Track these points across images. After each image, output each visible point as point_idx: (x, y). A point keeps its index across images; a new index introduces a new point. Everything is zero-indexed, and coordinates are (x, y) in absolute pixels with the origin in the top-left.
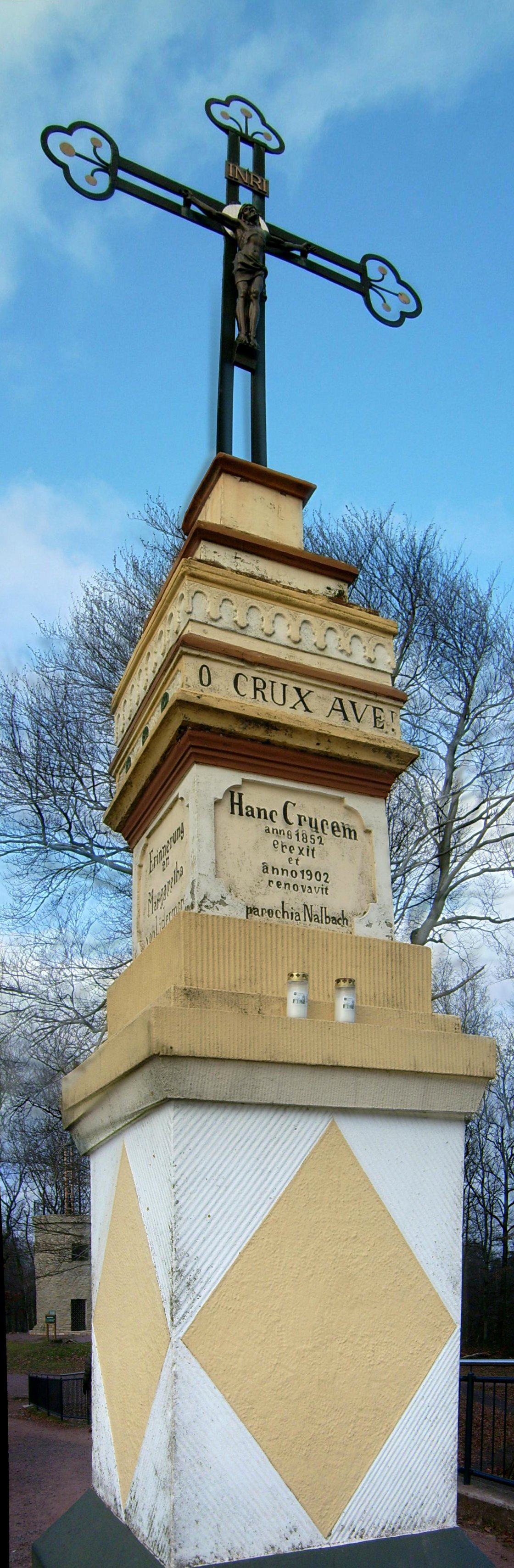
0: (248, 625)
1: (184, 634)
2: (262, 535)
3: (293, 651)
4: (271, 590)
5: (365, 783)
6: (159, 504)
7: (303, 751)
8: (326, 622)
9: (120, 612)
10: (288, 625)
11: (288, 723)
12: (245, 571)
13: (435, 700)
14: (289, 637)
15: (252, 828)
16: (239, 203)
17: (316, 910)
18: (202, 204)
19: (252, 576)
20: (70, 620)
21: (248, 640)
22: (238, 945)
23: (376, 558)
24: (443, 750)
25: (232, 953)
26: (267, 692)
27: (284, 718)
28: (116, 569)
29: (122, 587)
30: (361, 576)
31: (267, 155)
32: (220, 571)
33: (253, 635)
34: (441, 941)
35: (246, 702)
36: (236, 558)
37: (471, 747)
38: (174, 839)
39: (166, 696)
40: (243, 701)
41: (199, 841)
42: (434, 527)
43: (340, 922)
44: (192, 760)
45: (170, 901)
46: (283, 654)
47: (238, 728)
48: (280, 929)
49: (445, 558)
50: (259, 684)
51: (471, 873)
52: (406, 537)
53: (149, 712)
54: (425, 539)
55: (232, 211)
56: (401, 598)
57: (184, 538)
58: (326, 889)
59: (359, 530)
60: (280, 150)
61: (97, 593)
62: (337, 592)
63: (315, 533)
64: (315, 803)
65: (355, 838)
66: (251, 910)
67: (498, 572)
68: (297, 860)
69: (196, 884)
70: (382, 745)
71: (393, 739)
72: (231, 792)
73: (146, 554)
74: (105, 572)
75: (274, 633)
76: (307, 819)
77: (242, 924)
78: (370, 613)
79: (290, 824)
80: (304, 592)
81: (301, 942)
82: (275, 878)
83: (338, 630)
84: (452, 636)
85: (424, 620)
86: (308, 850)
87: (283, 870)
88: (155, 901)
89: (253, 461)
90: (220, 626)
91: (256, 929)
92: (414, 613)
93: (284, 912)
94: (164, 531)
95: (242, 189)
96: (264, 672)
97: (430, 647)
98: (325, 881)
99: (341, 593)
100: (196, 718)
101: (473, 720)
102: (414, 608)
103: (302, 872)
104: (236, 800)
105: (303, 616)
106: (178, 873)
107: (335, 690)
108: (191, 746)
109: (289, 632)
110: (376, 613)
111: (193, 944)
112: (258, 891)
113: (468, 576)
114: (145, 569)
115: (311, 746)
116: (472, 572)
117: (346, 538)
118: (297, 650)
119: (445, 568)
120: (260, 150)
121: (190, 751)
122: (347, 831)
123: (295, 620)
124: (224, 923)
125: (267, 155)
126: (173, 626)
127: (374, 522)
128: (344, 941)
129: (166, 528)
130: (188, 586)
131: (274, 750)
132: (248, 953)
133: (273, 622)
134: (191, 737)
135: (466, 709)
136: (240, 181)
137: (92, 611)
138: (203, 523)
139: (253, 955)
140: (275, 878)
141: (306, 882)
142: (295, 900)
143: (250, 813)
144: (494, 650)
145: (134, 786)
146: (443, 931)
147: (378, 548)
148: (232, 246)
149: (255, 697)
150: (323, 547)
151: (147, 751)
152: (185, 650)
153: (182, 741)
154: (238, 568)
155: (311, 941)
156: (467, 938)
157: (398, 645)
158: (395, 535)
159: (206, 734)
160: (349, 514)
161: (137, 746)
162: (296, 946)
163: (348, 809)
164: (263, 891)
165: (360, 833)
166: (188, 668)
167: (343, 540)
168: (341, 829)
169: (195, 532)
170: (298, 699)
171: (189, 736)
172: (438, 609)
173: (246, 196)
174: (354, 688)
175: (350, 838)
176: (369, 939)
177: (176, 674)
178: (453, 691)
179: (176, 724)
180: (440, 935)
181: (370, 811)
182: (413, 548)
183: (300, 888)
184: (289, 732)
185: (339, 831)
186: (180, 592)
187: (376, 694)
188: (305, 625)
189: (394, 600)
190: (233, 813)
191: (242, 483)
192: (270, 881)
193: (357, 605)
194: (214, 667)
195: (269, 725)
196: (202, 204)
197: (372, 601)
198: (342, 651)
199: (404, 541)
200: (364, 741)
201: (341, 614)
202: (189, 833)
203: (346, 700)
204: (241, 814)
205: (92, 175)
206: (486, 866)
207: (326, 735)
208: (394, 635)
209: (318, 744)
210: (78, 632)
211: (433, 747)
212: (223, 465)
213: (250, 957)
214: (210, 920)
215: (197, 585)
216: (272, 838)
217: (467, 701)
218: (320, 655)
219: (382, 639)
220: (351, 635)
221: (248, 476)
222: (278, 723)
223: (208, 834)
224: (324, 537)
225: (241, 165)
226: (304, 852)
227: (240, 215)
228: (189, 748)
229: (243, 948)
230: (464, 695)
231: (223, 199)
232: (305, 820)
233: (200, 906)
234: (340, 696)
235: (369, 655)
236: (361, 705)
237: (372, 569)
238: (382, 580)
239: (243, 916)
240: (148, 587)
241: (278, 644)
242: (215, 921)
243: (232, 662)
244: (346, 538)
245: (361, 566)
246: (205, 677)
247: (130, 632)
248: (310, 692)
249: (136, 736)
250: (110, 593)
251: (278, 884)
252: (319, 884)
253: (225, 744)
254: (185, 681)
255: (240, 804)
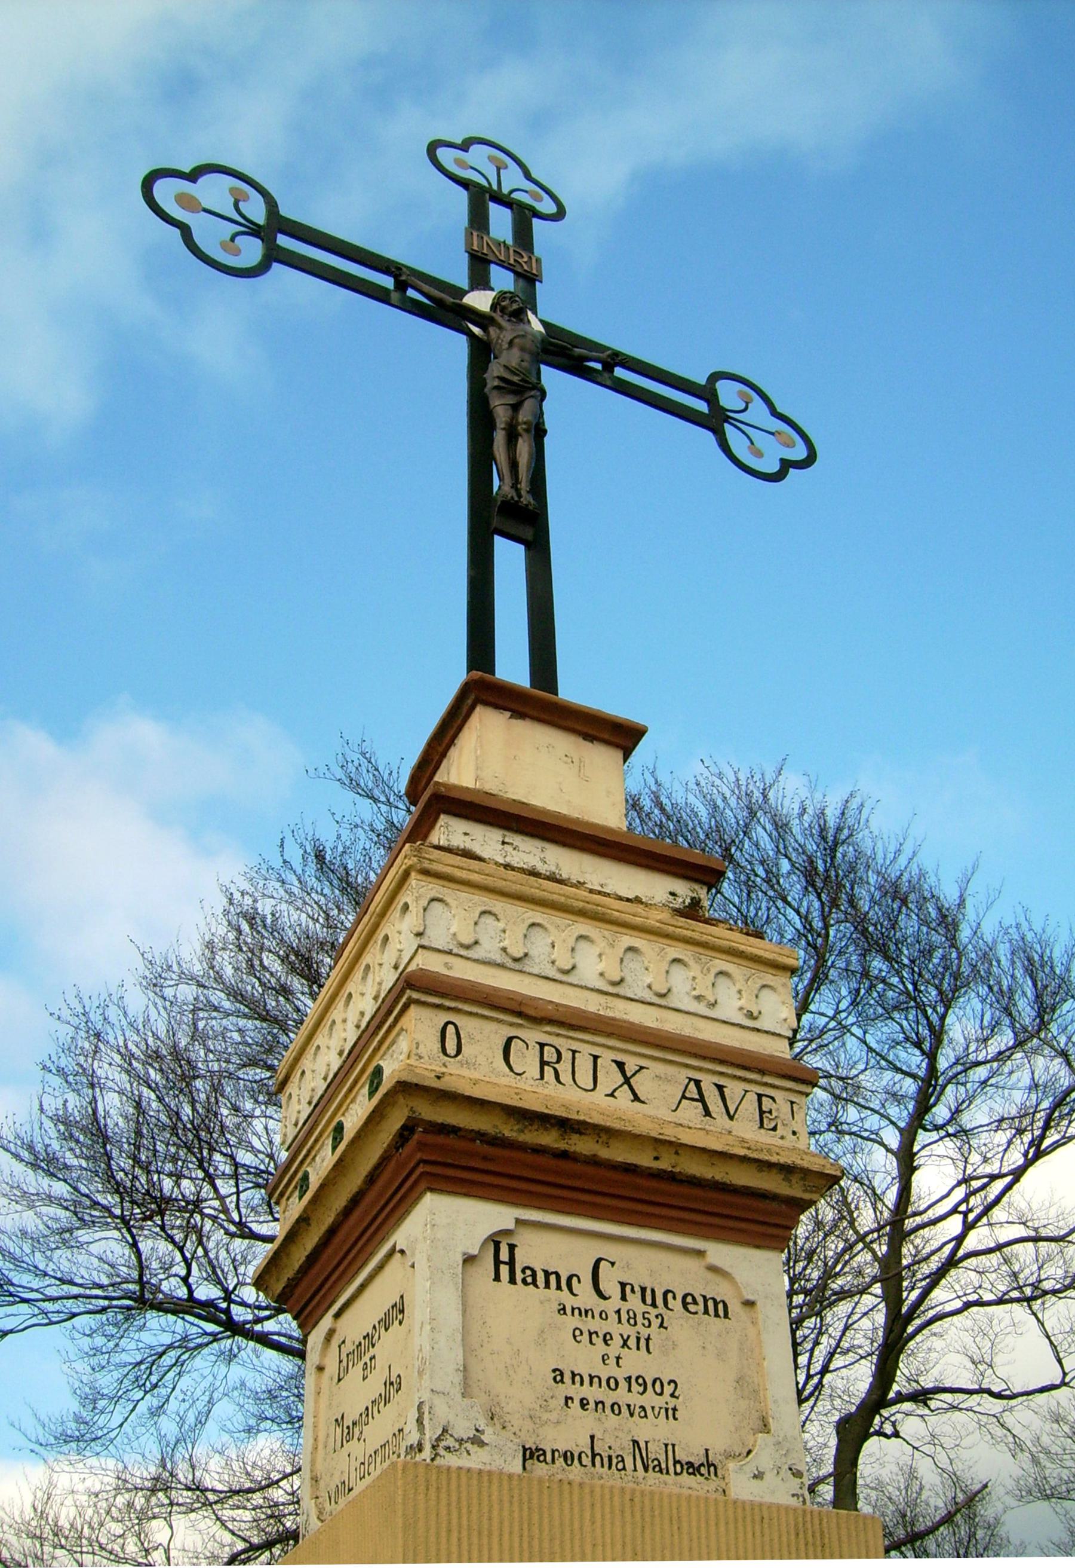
0: (526, 955)
1: (409, 969)
2: (552, 806)
3: (610, 998)
4: (568, 897)
5: (743, 1225)
6: (363, 754)
7: (630, 1169)
8: (668, 949)
9: (290, 933)
10: (600, 955)
11: (603, 1123)
12: (521, 865)
13: (870, 1057)
14: (601, 974)
15: (537, 1301)
16: (492, 289)
17: (656, 1451)
18: (426, 288)
19: (534, 873)
20: (198, 947)
21: (527, 980)
22: (506, 1524)
23: (757, 845)
24: (893, 1139)
25: (495, 1539)
26: (564, 1067)
27: (594, 1114)
28: (285, 862)
29: (296, 891)
30: (730, 875)
31: (536, 222)
32: (474, 864)
33: (536, 971)
34: (896, 1434)
35: (525, 1084)
36: (503, 843)
37: (942, 1133)
38: (386, 1323)
39: (378, 1071)
40: (522, 1084)
41: (432, 1330)
42: (858, 794)
43: (703, 1470)
44: (423, 1185)
45: (377, 1432)
46: (593, 1004)
47: (509, 1130)
48: (587, 1490)
49: (879, 844)
50: (550, 1055)
51: (948, 1308)
52: (810, 811)
53: (346, 1096)
54: (843, 814)
55: (480, 301)
56: (803, 911)
57: (408, 811)
58: (675, 1409)
59: (725, 799)
60: (560, 215)
61: (248, 900)
62: (688, 901)
63: (647, 803)
64: (652, 1257)
65: (726, 1316)
66: (531, 1454)
67: (975, 868)
68: (618, 1358)
69: (426, 1409)
70: (774, 1159)
71: (794, 1149)
72: (494, 1241)
73: (339, 837)
74: (264, 867)
75: (574, 968)
76: (637, 1289)
77: (515, 1483)
78: (747, 934)
79: (605, 1298)
80: (628, 900)
81: (628, 1514)
82: (578, 1392)
83: (691, 963)
84: (898, 972)
85: (846, 946)
86: (638, 1339)
87: (591, 1378)
88: (349, 1430)
89: (533, 684)
90: (476, 956)
91: (541, 1492)
92: (827, 935)
93: (594, 1455)
94: (372, 798)
95: (494, 269)
96: (558, 1035)
97: (858, 991)
98: (672, 1395)
99: (696, 903)
100: (429, 1112)
101: (943, 1087)
102: (826, 927)
103: (629, 1379)
104: (504, 1256)
105: (628, 940)
106: (394, 1384)
107: (687, 1066)
108: (426, 1162)
109: (601, 967)
110: (760, 935)
111: (421, 1524)
112: (545, 1416)
113: (922, 875)
114: (337, 862)
115: (644, 1159)
116: (929, 866)
117: (703, 812)
118: (617, 996)
119: (880, 861)
120: (524, 217)
121: (420, 1169)
122: (710, 1304)
123: (612, 946)
124: (480, 1481)
125: (536, 222)
126: (389, 957)
127: (751, 787)
128: (712, 1510)
129: (377, 793)
130: (418, 890)
131: (578, 1167)
132: (525, 1539)
133: (573, 949)
134: (422, 1146)
135: (932, 1068)
136: (491, 257)
137: (239, 931)
138: (444, 785)
139: (536, 1543)
140: (578, 1392)
141: (635, 1399)
142: (615, 1431)
143: (529, 1280)
144: (973, 995)
145: (313, 1223)
146: (899, 1416)
147: (759, 829)
148: (481, 354)
149: (542, 1078)
150: (661, 826)
151: (340, 1167)
152: (415, 995)
153: (405, 1151)
154: (508, 859)
155: (647, 1514)
156: (947, 1429)
157: (800, 986)
158: (790, 807)
159: (451, 1141)
160: (706, 773)
161: (322, 1154)
162: (618, 1523)
163: (713, 1269)
164: (554, 1416)
165: (734, 1307)
166: (420, 1028)
167: (696, 815)
168: (700, 1300)
169: (431, 799)
170: (621, 1080)
171: (419, 1143)
172: (871, 929)
173: (502, 280)
174: (722, 1062)
175: (717, 1315)
176: (761, 1505)
177: (398, 1034)
178: (907, 1039)
179: (395, 1122)
180: (894, 1424)
181: (757, 1272)
182: (823, 830)
183: (624, 1409)
184: (604, 1137)
185: (695, 1302)
186: (405, 897)
187: (762, 1072)
188: (630, 955)
189: (791, 914)
190: (497, 1278)
191: (514, 721)
192: (567, 1399)
193: (724, 921)
194: (467, 1025)
195: (565, 1125)
196: (426, 288)
197: (752, 915)
198: (698, 998)
199: (805, 817)
200: (742, 1152)
201: (696, 936)
202: (417, 1313)
203: (708, 1082)
204: (512, 1280)
205: (233, 239)
206: (973, 1297)
207: (671, 1143)
208: (793, 971)
209: (656, 1158)
210: (212, 967)
211: (872, 1133)
212: (481, 691)
213: (530, 1546)
214: (454, 1475)
215: (434, 888)
216: (573, 1321)
217: (932, 1057)
218: (660, 1006)
219: (769, 978)
220: (714, 971)
221: (521, 709)
222: (584, 1123)
223: (452, 1317)
224: (662, 810)
225: (491, 235)
226: (632, 1342)
227: (494, 307)
228: (418, 1164)
229: (516, 1528)
230: (926, 1046)
231: (463, 283)
232: (633, 1291)
233: (433, 1447)
234: (697, 1076)
235: (747, 1005)
236: (734, 1089)
237: (750, 863)
238: (768, 881)
239: (516, 1466)
240: (343, 890)
241: (581, 987)
242: (464, 1479)
243: (501, 1016)
244: (703, 812)
245: (731, 858)
246: (451, 1043)
247: (310, 967)
248: (642, 1068)
249: (356, 1082)
250: (273, 902)
251: (584, 1403)
252: (659, 1401)
253: (485, 1158)
254: (413, 1049)
255: (511, 1263)
